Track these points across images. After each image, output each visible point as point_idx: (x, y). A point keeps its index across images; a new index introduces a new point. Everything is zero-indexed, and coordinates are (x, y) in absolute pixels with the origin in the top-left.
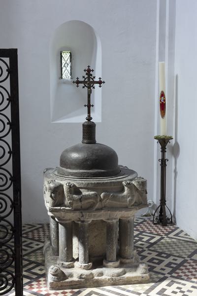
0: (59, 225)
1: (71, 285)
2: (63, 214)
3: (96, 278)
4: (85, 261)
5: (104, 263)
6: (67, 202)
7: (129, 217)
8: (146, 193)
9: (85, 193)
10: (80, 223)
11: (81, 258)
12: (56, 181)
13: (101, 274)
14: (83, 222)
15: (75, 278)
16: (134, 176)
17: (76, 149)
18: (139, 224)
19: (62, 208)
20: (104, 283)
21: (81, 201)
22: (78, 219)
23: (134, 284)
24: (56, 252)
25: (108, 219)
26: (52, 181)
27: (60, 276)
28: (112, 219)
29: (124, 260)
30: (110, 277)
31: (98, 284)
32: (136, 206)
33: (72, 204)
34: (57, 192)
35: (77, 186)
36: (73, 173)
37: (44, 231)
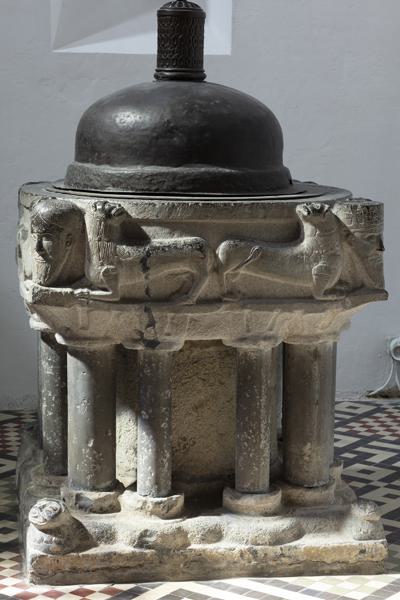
1: (108, 569)
3: (195, 546)
4: (158, 488)
5: (227, 499)
6: (97, 269)
7: (318, 337)
8: (381, 248)
9: (160, 238)
10: (140, 347)
11: (145, 479)
13: (216, 535)
14: (152, 344)
15: (123, 546)
16: (386, 509)
17: (132, 98)
18: (357, 418)
19: (78, 291)
20: (223, 565)
21: (146, 269)
23: (332, 573)
24: (58, 465)
25: (243, 340)
27: (71, 537)
28: (256, 339)
29: (296, 493)
30: (244, 547)
31: (205, 569)
32: (342, 293)
33: (116, 278)
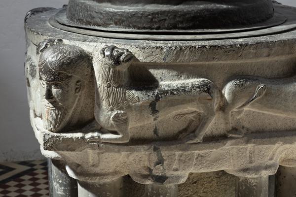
0: (80, 189)
2: (91, 155)
6: (107, 114)
12: (66, 42)
14: (161, 179)
19: (88, 136)
22: (147, 173)
25: (245, 170)
26: (51, 41)
28: (257, 169)
33: (126, 121)
34: (70, 74)
35: (141, 57)
36: (122, 14)
37: (34, 183)
